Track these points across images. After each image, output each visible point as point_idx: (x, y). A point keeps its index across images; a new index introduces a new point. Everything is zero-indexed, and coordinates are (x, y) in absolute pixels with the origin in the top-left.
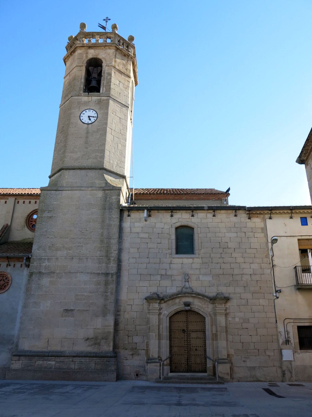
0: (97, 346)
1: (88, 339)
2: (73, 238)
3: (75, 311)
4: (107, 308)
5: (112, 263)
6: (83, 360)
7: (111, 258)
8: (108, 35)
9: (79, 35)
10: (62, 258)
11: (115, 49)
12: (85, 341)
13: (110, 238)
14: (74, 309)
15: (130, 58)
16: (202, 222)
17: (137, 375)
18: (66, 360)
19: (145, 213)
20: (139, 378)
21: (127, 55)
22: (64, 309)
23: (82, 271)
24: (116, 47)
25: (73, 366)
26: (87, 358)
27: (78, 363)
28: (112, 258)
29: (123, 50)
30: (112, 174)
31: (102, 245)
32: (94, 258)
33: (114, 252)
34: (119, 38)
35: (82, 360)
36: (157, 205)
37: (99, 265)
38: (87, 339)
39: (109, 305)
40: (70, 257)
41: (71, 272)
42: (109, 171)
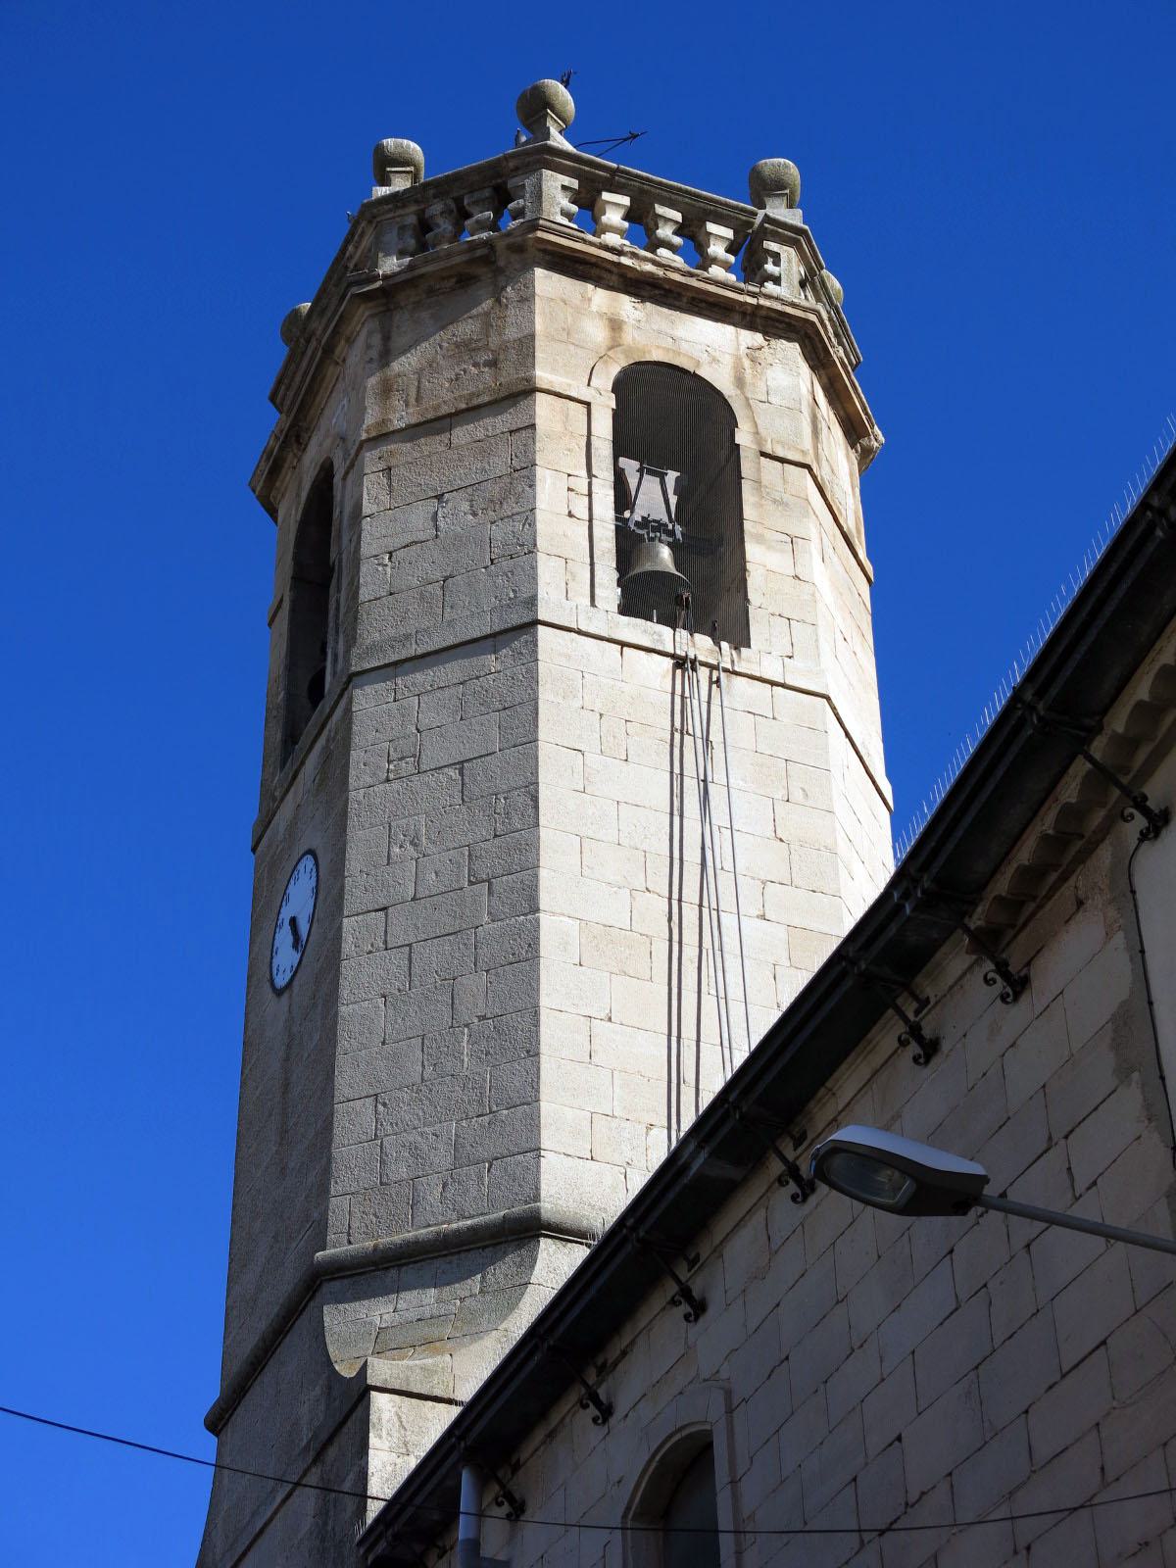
8: (354, 262)
9: (246, 1071)
11: (372, 316)
15: (514, 257)
16: (1080, 759)
19: (897, 1443)
21: (472, 262)
24: (368, 297)
29: (423, 270)
30: (408, 1274)
34: (413, 208)
36: (677, 968)
42: (374, 1263)
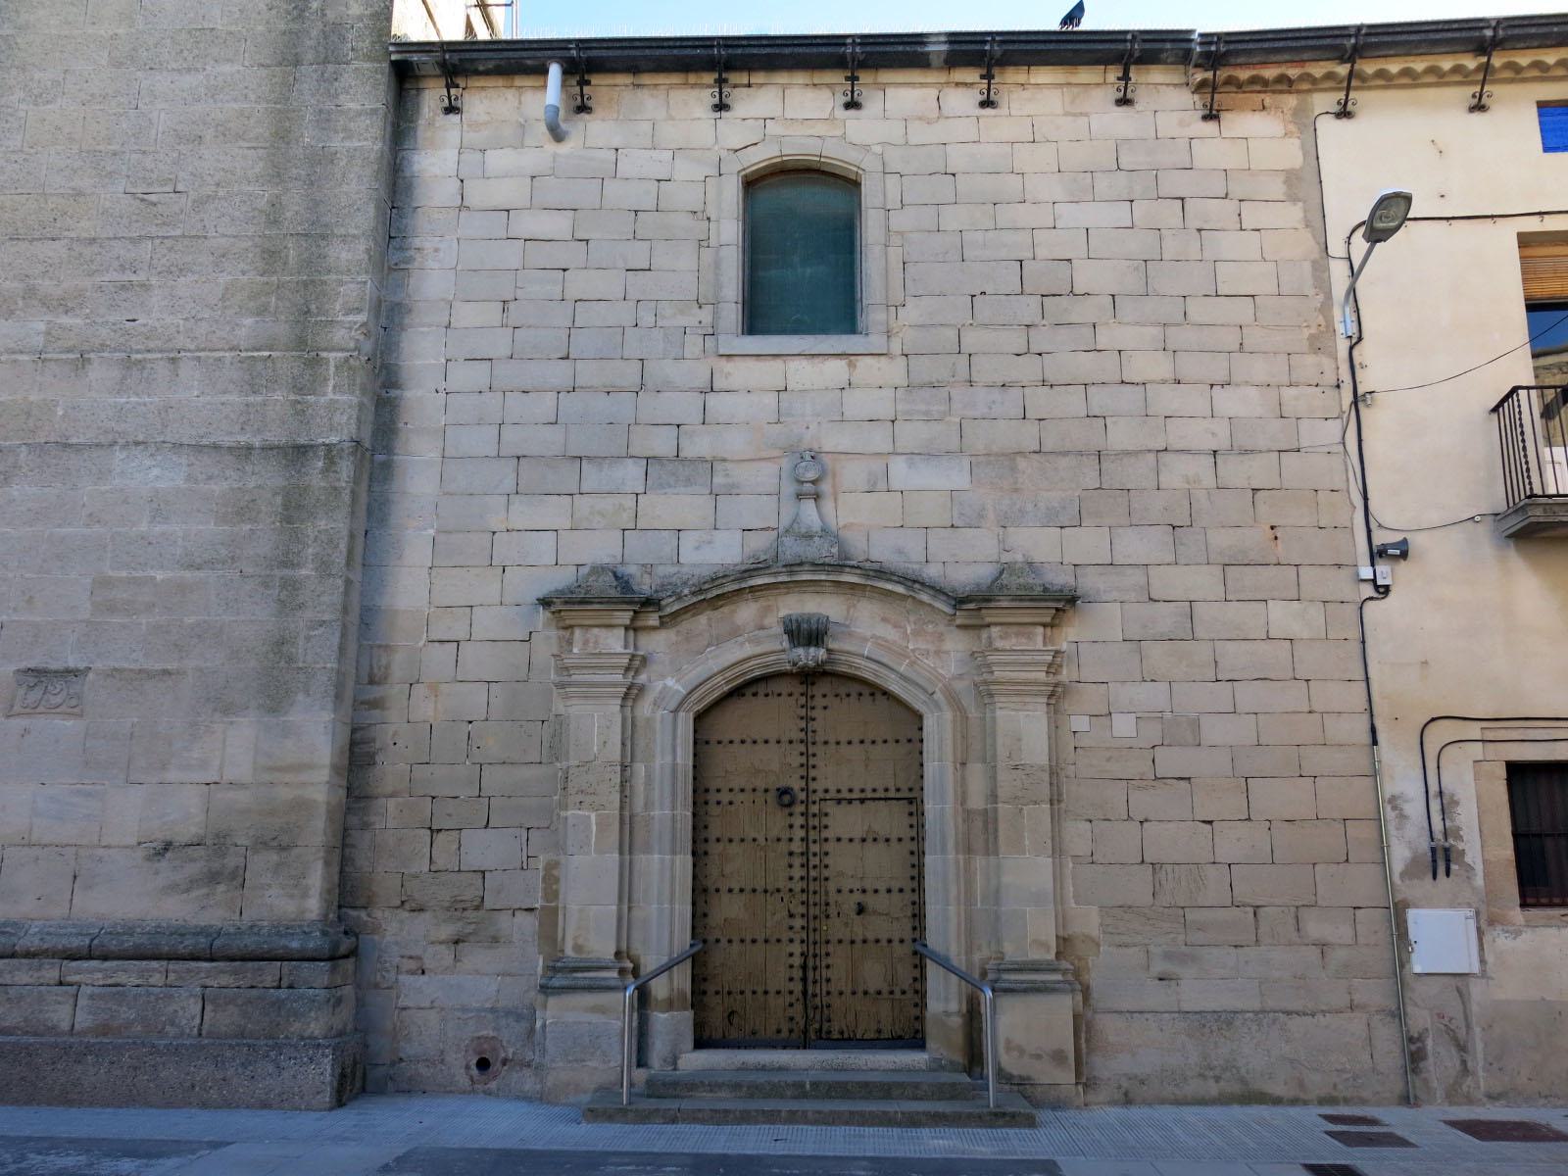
0: (221, 888)
1: (168, 846)
2: (93, 241)
3: (91, 676)
4: (291, 659)
5: (331, 383)
6: (128, 974)
7: (324, 354)
10: (20, 357)
12: (148, 859)
13: (323, 237)
14: (82, 666)
17: (483, 1064)
18: (23, 977)
20: (493, 1085)
22: (24, 665)
23: (141, 438)
25: (60, 1015)
26: (154, 964)
27: (91, 997)
28: (333, 357)
31: (274, 278)
32: (219, 359)
33: (351, 318)
35: (121, 978)
37: (251, 399)
38: (159, 846)
39: (308, 639)
40: (69, 351)
41: (74, 440)
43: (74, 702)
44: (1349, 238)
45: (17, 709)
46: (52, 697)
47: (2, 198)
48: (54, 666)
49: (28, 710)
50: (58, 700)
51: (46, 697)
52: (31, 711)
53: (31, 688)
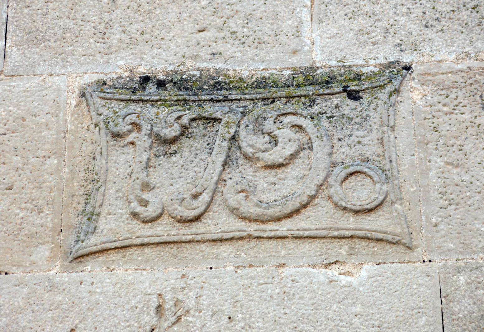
3: (414, 93)
14: (368, 59)
22: (120, 65)
43: (362, 193)
44: (370, 210)
45: (113, 224)
46: (262, 180)
47: (2, 169)
48: (246, 64)
49: (164, 230)
50: (292, 185)
51: (234, 176)
52: (184, 231)
53: (167, 144)
